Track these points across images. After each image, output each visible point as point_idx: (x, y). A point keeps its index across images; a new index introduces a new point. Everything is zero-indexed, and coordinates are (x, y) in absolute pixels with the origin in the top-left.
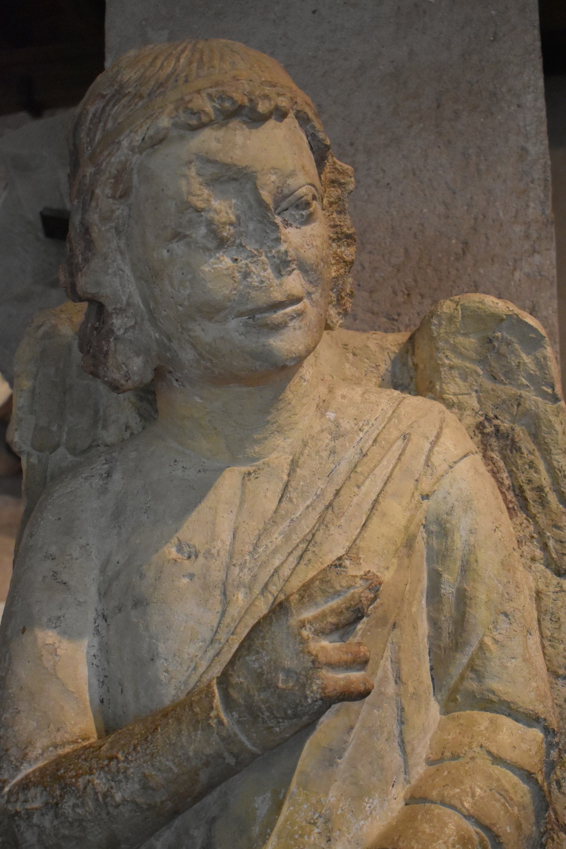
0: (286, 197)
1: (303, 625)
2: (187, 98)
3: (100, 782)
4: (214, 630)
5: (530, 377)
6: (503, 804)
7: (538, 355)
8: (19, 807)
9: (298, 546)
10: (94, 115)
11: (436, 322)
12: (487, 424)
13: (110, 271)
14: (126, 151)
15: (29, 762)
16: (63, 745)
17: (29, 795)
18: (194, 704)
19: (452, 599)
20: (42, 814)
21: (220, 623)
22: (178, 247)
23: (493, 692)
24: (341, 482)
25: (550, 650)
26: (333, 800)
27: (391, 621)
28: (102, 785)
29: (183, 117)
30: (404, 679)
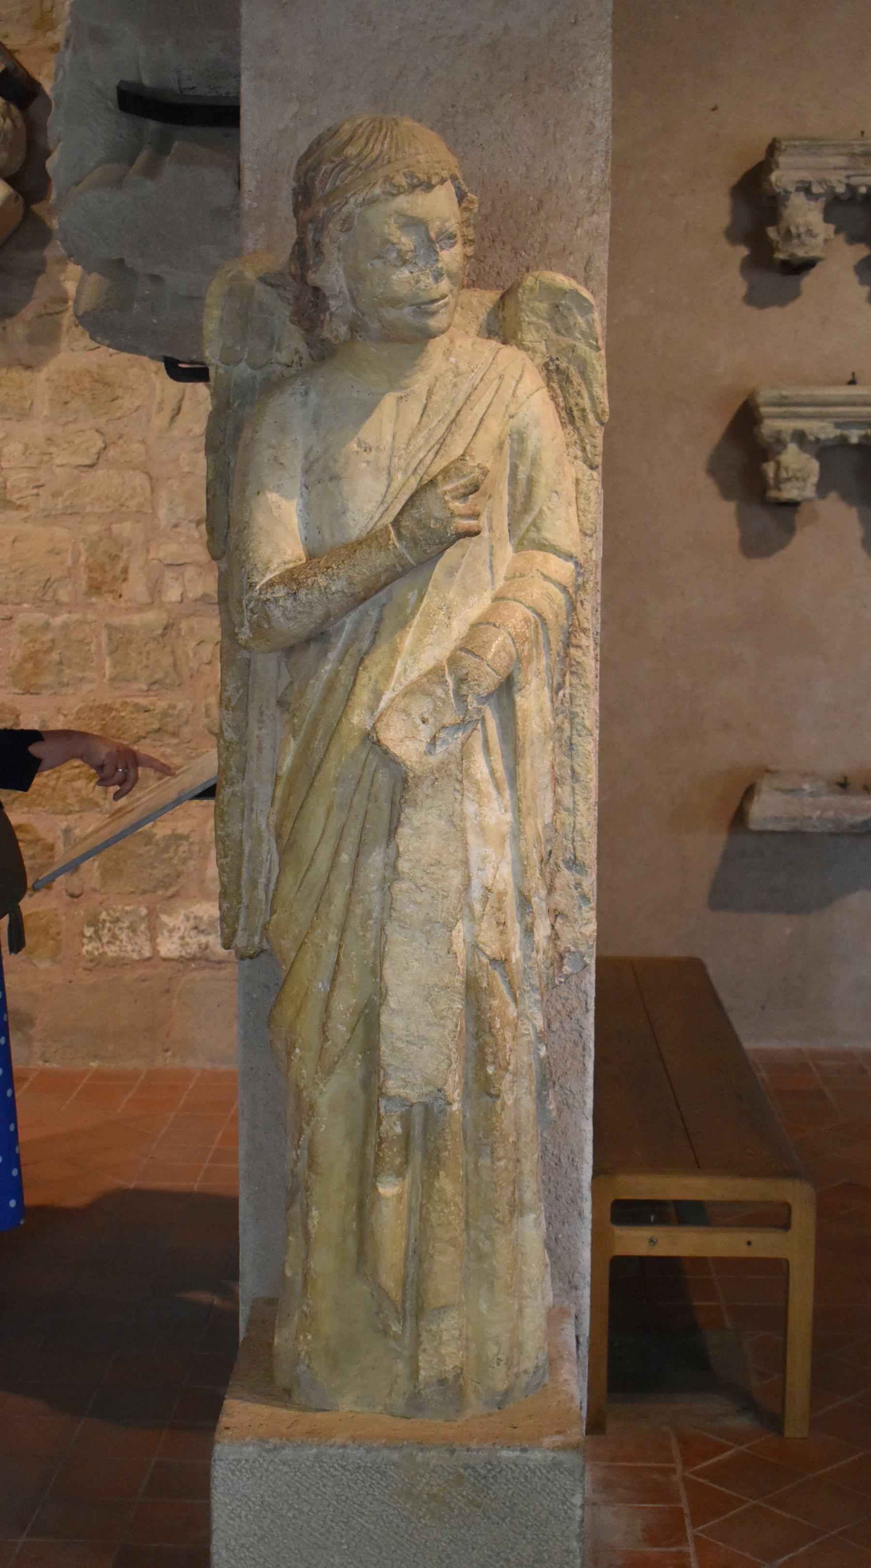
0: (443, 233)
2: (391, 176)
3: (322, 581)
5: (583, 333)
7: (589, 317)
8: (268, 596)
16: (289, 562)
19: (524, 482)
21: (387, 491)
22: (378, 263)
23: (546, 540)
25: (582, 518)
30: (494, 528)
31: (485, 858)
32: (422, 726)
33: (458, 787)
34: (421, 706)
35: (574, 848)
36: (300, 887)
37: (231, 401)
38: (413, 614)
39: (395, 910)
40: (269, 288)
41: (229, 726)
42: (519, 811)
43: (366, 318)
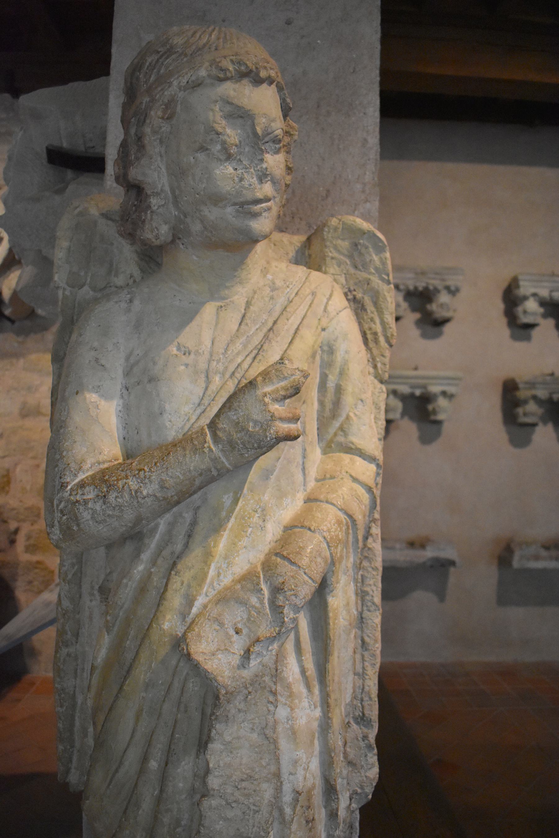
0: (269, 134)
1: (265, 395)
2: (218, 60)
3: (133, 484)
4: (201, 398)
5: (376, 269)
6: (358, 504)
8: (78, 498)
9: (252, 351)
10: (150, 64)
11: (327, 230)
12: (349, 294)
13: (152, 167)
14: (175, 88)
15: (83, 472)
16: (104, 462)
17: (85, 491)
18: (194, 440)
20: (95, 502)
21: (204, 393)
22: (201, 156)
23: (353, 443)
24: (276, 317)
26: (267, 498)
27: (303, 399)
28: (134, 485)
29: (214, 72)
31: (296, 762)
32: (235, 637)
33: (271, 699)
34: (235, 615)
35: (363, 707)
36: (109, 785)
37: (75, 318)
38: (228, 518)
39: (204, 827)
40: (110, 222)
41: (66, 596)
42: (328, 707)
43: (188, 220)
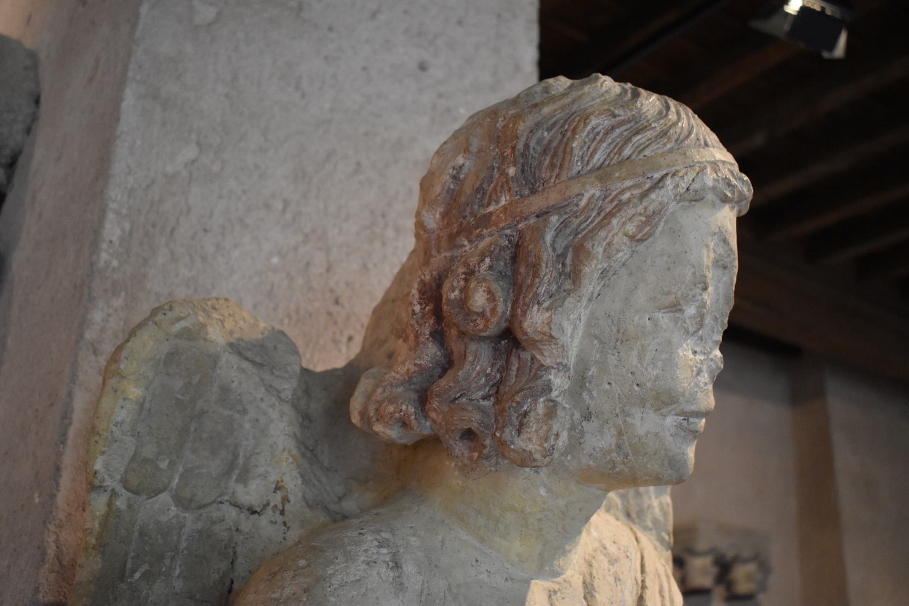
22: (664, 319)
37: (129, 565)
